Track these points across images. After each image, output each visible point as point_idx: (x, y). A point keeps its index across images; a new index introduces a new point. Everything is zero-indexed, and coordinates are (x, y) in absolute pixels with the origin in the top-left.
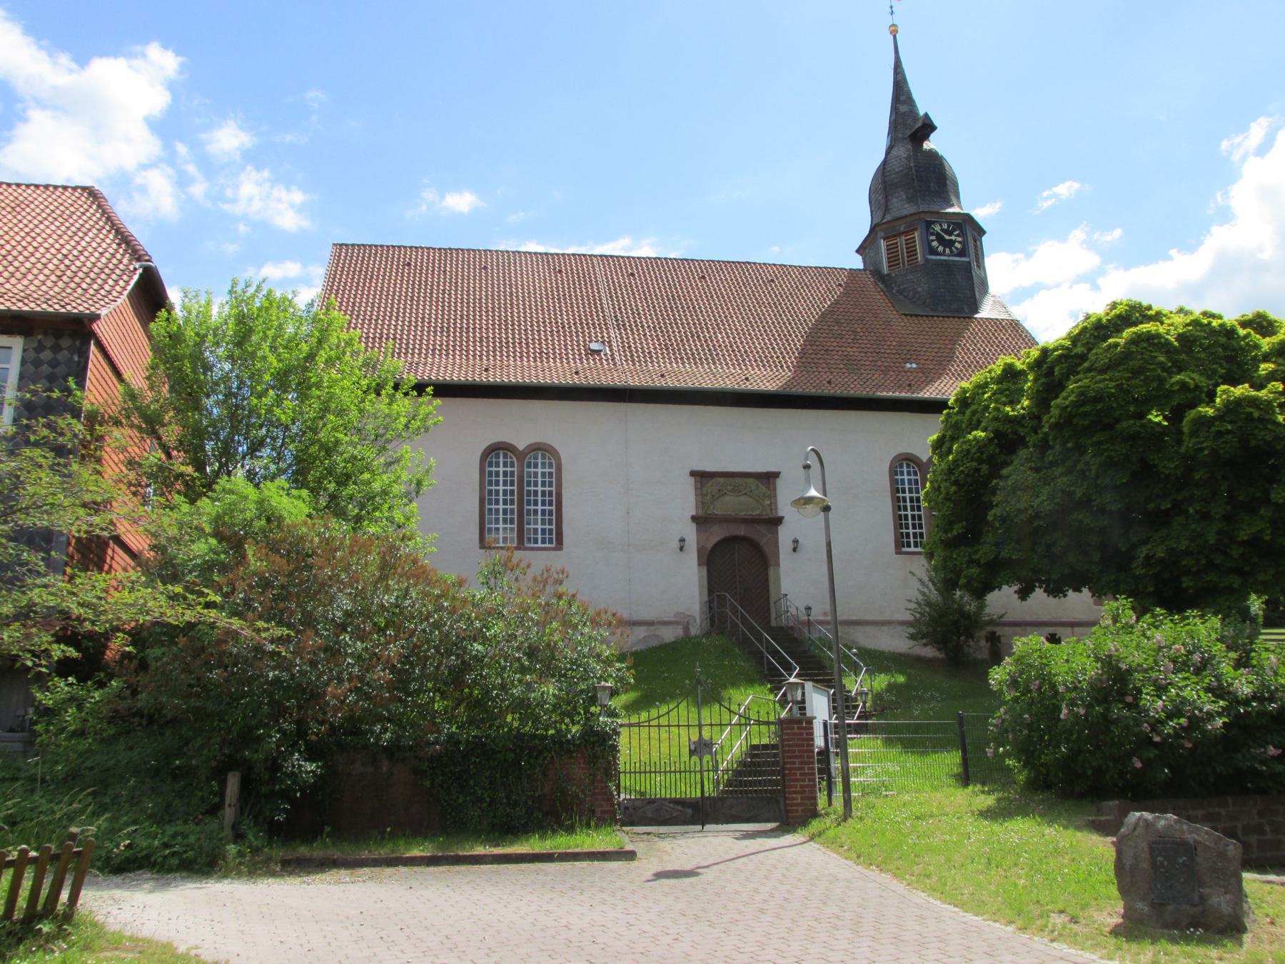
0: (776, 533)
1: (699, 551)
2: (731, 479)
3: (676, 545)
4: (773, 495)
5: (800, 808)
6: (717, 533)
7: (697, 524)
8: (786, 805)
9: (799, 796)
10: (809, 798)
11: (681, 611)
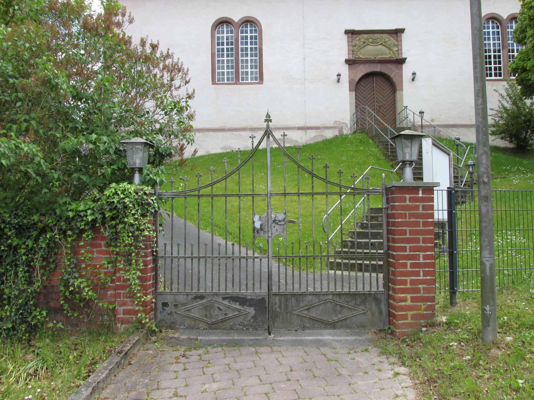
0: (401, 69)
1: (350, 82)
2: (371, 35)
3: (336, 78)
4: (399, 45)
5: (410, 313)
6: (363, 70)
7: (349, 64)
8: (389, 305)
9: (409, 296)
10: (424, 300)
11: (338, 120)
